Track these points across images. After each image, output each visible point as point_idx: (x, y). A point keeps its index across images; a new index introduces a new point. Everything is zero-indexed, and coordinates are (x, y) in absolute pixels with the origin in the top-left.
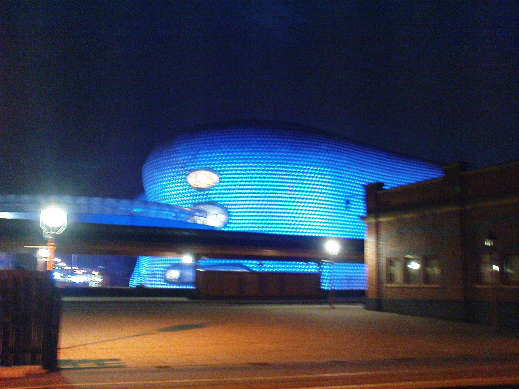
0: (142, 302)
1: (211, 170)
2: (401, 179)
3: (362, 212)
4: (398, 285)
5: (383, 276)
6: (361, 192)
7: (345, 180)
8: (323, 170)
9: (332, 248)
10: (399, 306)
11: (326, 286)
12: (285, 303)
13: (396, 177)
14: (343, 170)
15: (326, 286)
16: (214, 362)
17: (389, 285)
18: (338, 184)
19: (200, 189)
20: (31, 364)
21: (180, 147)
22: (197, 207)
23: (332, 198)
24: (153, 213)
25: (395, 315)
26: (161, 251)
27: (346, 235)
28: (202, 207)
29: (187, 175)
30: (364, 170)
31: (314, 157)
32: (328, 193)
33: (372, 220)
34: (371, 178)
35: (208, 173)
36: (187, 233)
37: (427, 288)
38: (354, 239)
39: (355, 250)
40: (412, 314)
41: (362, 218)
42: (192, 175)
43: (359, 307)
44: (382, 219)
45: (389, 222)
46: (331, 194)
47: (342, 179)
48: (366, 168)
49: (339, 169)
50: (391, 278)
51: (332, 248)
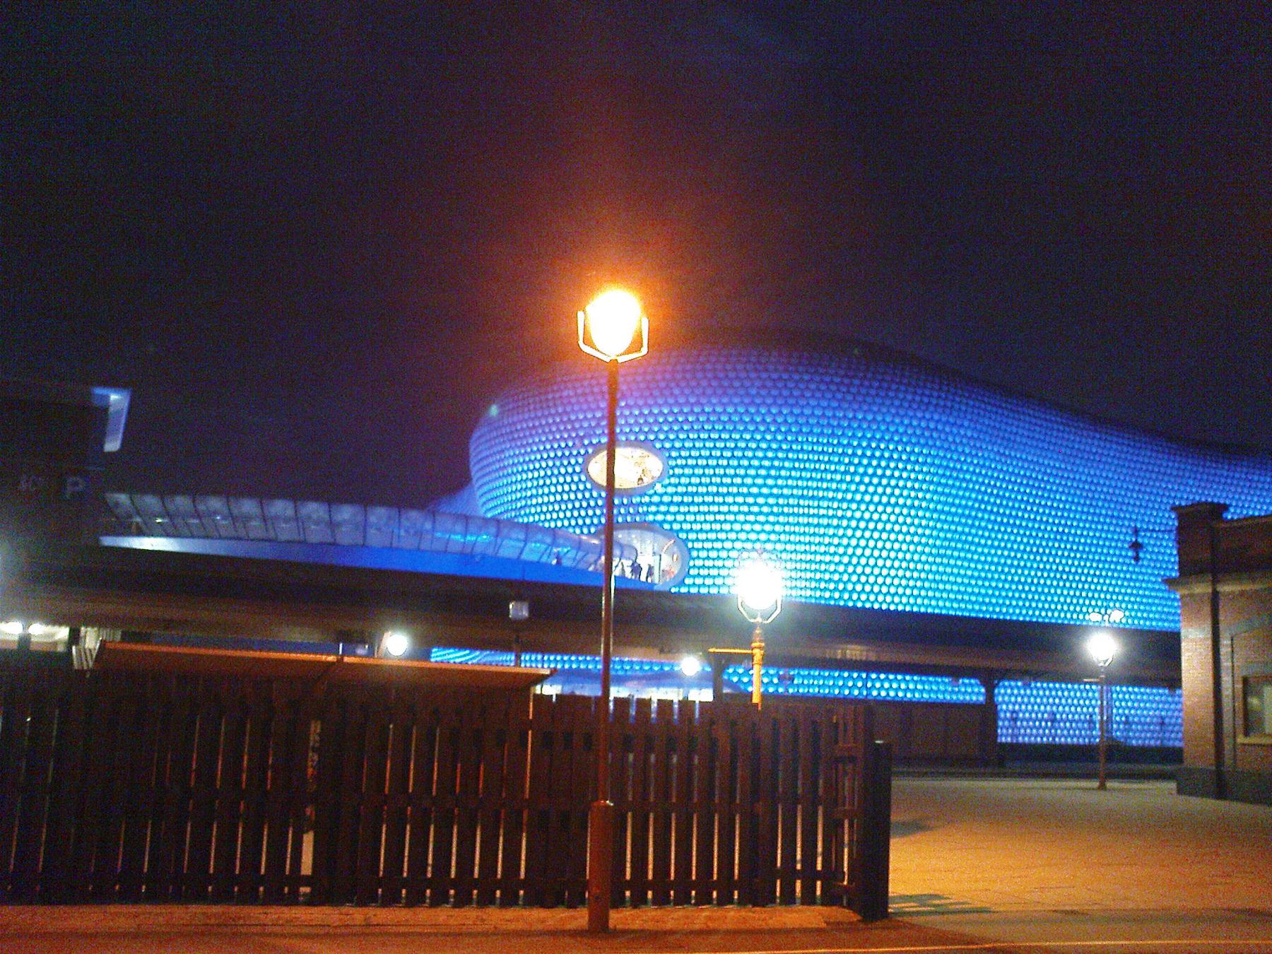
9: (1102, 649)
33: (1202, 589)
34: (1193, 492)
39: (1156, 658)
44: (1225, 588)
51: (1102, 649)
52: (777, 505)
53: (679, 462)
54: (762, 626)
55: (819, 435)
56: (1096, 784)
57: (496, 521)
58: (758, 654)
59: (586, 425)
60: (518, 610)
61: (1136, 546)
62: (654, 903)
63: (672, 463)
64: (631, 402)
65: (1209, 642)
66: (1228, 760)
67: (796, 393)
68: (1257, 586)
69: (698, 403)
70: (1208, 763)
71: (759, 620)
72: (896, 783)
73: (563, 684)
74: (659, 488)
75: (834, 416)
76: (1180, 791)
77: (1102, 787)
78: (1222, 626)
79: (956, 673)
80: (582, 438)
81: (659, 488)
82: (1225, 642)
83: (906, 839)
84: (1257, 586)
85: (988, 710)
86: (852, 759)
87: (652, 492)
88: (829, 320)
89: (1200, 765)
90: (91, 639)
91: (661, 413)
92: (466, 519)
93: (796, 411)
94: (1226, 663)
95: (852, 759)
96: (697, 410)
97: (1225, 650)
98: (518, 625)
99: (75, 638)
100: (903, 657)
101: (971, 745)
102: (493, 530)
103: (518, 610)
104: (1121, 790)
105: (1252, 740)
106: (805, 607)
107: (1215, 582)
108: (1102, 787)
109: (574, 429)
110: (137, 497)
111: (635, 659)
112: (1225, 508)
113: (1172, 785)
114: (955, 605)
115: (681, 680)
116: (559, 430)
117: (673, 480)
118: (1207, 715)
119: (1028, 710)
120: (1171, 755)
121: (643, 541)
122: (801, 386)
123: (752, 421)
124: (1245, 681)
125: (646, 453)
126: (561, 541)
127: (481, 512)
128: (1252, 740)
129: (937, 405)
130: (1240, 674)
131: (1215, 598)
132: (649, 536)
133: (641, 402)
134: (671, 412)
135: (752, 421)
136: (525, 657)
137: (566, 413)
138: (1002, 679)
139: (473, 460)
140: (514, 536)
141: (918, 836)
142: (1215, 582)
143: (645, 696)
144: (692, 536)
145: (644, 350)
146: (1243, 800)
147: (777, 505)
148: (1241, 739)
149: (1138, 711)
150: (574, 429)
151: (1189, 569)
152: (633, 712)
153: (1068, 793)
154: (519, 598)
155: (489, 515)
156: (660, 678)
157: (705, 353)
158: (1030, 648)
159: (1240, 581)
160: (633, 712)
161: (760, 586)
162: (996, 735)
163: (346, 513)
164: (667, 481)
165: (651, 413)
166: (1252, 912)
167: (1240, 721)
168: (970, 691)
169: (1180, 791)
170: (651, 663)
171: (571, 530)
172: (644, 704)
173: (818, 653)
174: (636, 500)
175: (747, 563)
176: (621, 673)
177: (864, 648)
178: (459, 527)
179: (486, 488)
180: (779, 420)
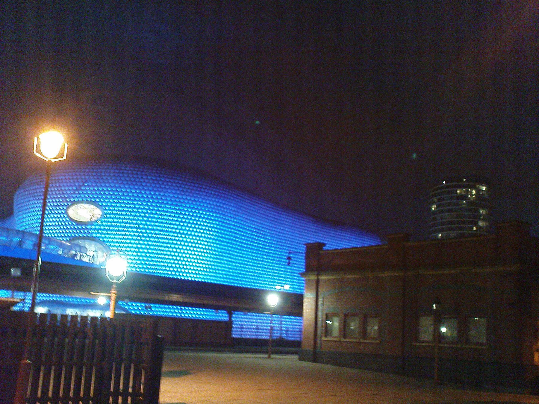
1: (95, 203)
2: (230, 221)
4: (335, 339)
5: (319, 329)
6: (303, 249)
7: (231, 227)
8: (222, 218)
9: (273, 300)
10: (334, 358)
11: (236, 334)
12: (172, 349)
14: (230, 217)
15: (236, 334)
18: (225, 230)
19: (79, 223)
22: (76, 242)
23: (218, 244)
25: (332, 367)
27: (216, 280)
28: (81, 242)
29: (68, 207)
30: (248, 218)
31: (204, 201)
32: (214, 239)
33: (313, 277)
34: (315, 238)
38: (288, 293)
39: (293, 304)
40: (347, 365)
41: (302, 274)
42: (73, 207)
44: (322, 278)
45: (329, 280)
46: (217, 240)
47: (229, 226)
48: (250, 216)
49: (227, 216)
50: (327, 330)
51: (273, 300)
52: (146, 233)
53: (109, 212)
54: (116, 284)
55: (161, 203)
56: (266, 356)
57: (23, 232)
59: (68, 192)
60: (15, 272)
61: (289, 258)
63: (106, 212)
64: (90, 184)
65: (314, 299)
66: (319, 345)
67: (162, 186)
68: (333, 277)
69: (120, 187)
70: (311, 348)
71: (115, 281)
72: (166, 354)
73: (49, 306)
74: (99, 222)
75: (178, 197)
76: (300, 359)
77: (269, 357)
78: (320, 293)
79: (217, 308)
80: (66, 198)
81: (99, 222)
82: (320, 299)
83: (178, 379)
85: (229, 325)
86: (147, 344)
87: (96, 224)
88: (141, 153)
89: (307, 349)
91: (103, 190)
92: (8, 230)
94: (320, 308)
95: (147, 344)
97: (320, 302)
98: (16, 279)
100: (192, 300)
101: (216, 340)
102: (21, 236)
103: (15, 272)
104: (280, 359)
105: (329, 339)
106: (137, 275)
107: (318, 275)
109: (63, 194)
111: (78, 297)
112: (324, 245)
113: (296, 357)
114: (195, 276)
115: (101, 307)
116: (56, 194)
118: (311, 328)
119: (245, 324)
120: (297, 344)
121: (90, 245)
122: (165, 183)
123: (147, 197)
124: (327, 315)
125: (95, 207)
126: (53, 243)
127: (17, 229)
128: (329, 339)
129: (218, 195)
130: (325, 312)
131: (318, 282)
132: (93, 243)
133: (94, 185)
134: (107, 190)
136: (16, 294)
137: (59, 186)
138: (237, 311)
139: (15, 204)
140: (30, 238)
141: (183, 378)
142: (318, 275)
143: (85, 314)
145: (65, 158)
146: (321, 362)
147: (146, 233)
148: (324, 338)
149: (287, 326)
150: (63, 194)
151: (309, 269)
152: (48, 319)
153: (249, 359)
154: (16, 266)
155: (21, 229)
156: (93, 306)
157: (142, 167)
158: (243, 298)
159: (327, 275)
160: (48, 319)
161: (116, 266)
162: (231, 334)
164: (103, 220)
165: (98, 190)
168: (222, 316)
169: (300, 359)
170: (85, 299)
171: (58, 238)
172: (64, 317)
173: (148, 296)
175: (113, 255)
176: (76, 303)
177: (178, 296)
178: (4, 234)
179: (20, 217)
180: (154, 197)
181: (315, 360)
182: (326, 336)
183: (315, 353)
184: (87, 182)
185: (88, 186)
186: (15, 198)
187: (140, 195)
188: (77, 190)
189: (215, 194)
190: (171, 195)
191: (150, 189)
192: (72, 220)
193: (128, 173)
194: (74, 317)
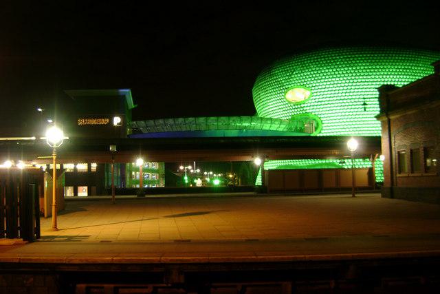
0: (191, 197)
3: (377, 111)
6: (377, 94)
9: (353, 145)
13: (401, 76)
16: (223, 238)
17: (398, 175)
19: (297, 104)
20: (389, 198)
21: (279, 70)
24: (267, 127)
25: (406, 201)
26: (241, 155)
35: (303, 90)
36: (252, 141)
37: (426, 176)
42: (289, 92)
43: (379, 195)
44: (392, 117)
45: (397, 119)
51: (353, 145)
58: (54, 157)
62: (7, 237)
63: (313, 91)
68: (414, 111)
71: (55, 146)
77: (354, 196)
82: (393, 138)
84: (414, 111)
90: (94, 166)
93: (396, 67)
94: (393, 147)
96: (319, 72)
97: (393, 141)
98: (112, 153)
99: (89, 167)
108: (354, 196)
110: (138, 122)
117: (314, 97)
129: (401, 59)
131: (389, 120)
135: (347, 73)
144: (322, 116)
146: (396, 198)
154: (113, 144)
163: (201, 120)
166: (307, 239)
167: (397, 169)
169: (383, 196)
174: (302, 106)
178: (259, 121)
181: (392, 197)
182: (400, 173)
183: (392, 189)
184: (294, 71)
185: (296, 74)
186: (254, 94)
187: (336, 73)
188: (289, 79)
189: (401, 59)
190: (362, 68)
191: (344, 66)
192: (289, 102)
193: (324, 57)
194: (353, 170)
